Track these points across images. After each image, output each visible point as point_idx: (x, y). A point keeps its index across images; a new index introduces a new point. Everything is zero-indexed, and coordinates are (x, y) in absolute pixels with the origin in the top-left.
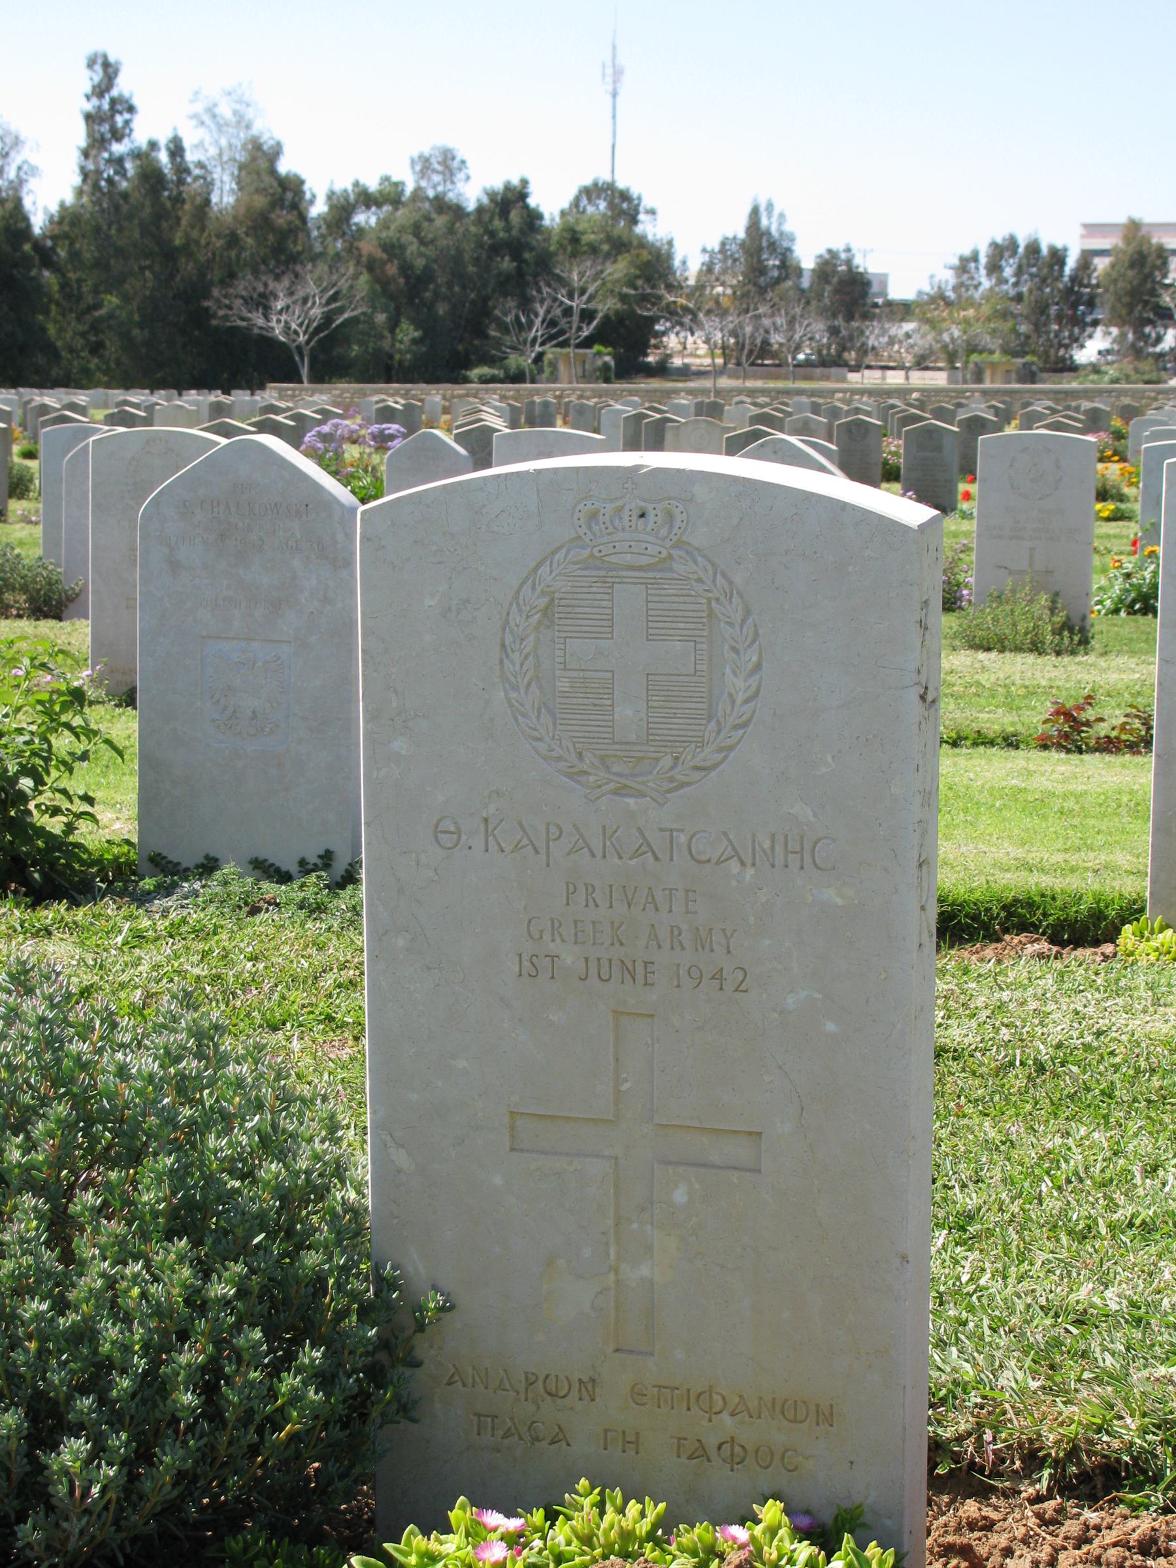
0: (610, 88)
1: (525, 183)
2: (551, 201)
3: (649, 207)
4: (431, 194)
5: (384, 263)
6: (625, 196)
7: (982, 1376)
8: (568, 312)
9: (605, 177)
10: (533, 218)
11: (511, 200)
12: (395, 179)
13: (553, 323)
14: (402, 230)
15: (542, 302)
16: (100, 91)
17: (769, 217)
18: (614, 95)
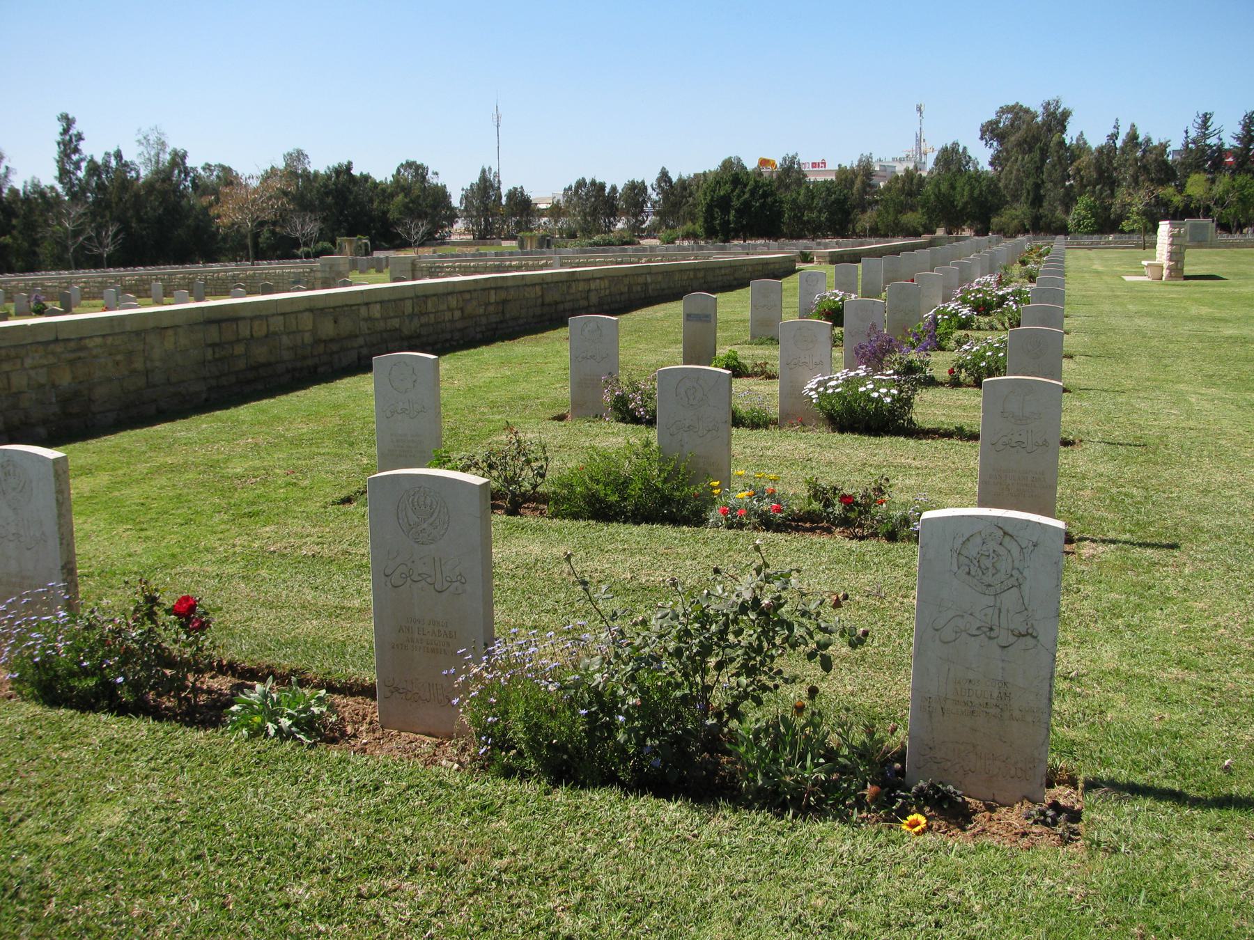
1: (350, 163)
16: (66, 131)
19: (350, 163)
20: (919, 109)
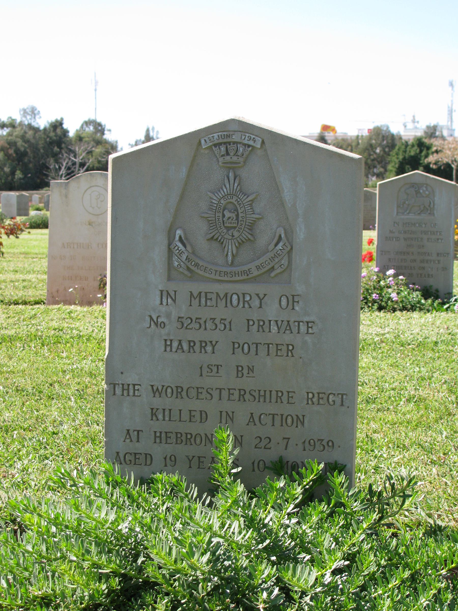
0: (94, 88)
1: (62, 119)
2: (72, 127)
3: (109, 128)
4: (26, 123)
5: (8, 149)
6: (100, 124)
7: (240, 561)
8: (74, 164)
9: (93, 118)
10: (65, 132)
11: (57, 125)
12: (13, 118)
13: (69, 168)
14: (17, 137)
15: (65, 160)
17: (153, 132)
18: (96, 90)
19: (62, 119)
20: (451, 84)
